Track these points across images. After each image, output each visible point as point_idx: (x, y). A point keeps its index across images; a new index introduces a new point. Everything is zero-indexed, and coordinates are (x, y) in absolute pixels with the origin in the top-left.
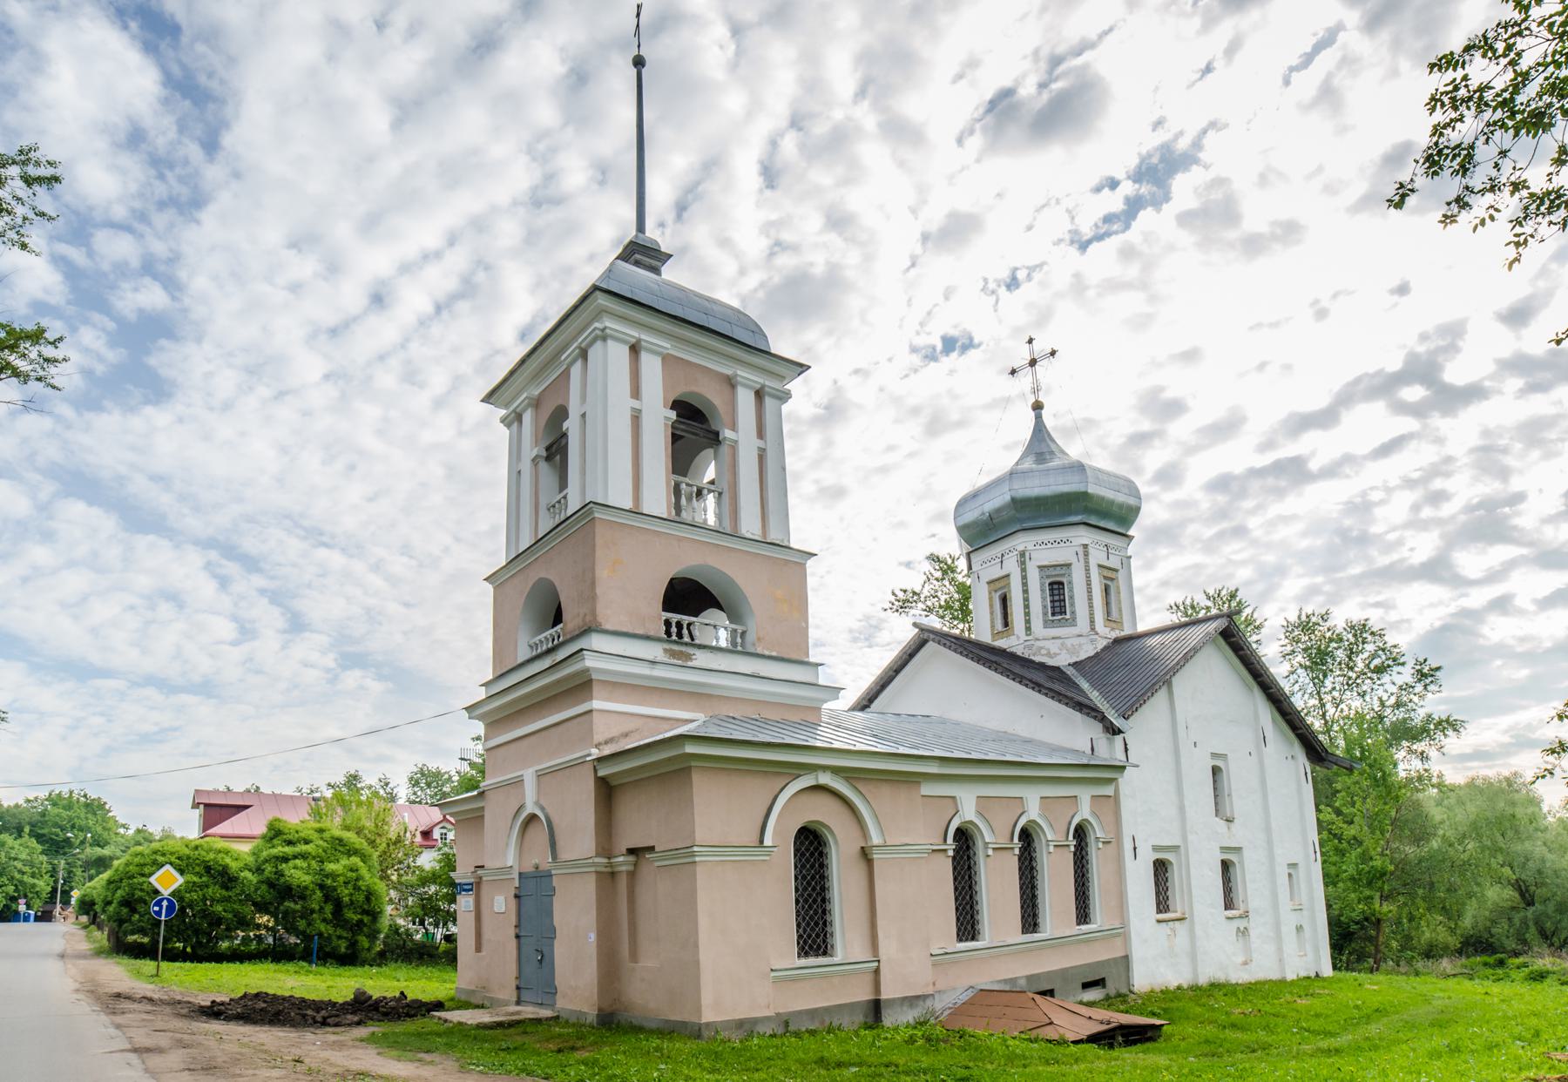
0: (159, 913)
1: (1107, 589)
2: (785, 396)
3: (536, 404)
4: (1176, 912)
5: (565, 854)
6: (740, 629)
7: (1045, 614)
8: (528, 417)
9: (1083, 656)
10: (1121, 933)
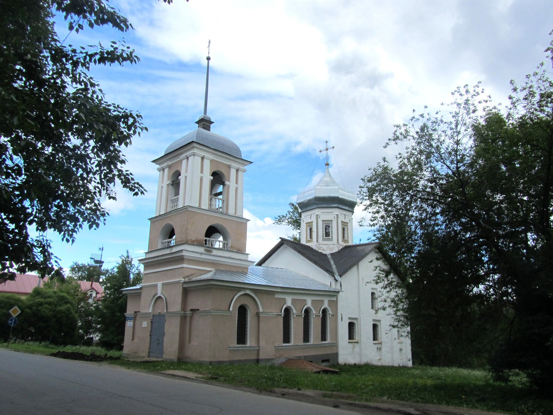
0: (11, 324)
1: (344, 229)
3: (170, 167)
4: (356, 340)
5: (170, 310)
6: (226, 242)
7: (323, 236)
8: (166, 170)
9: (334, 251)
10: (335, 345)
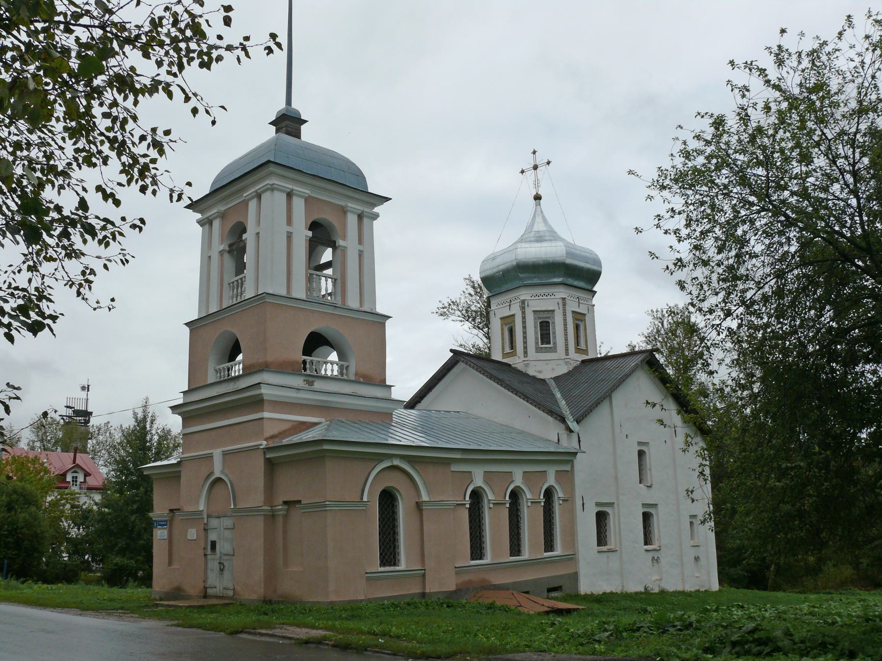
1: (577, 328)
2: (376, 216)
3: (223, 216)
7: (537, 343)
8: (216, 224)
10: (571, 558)
